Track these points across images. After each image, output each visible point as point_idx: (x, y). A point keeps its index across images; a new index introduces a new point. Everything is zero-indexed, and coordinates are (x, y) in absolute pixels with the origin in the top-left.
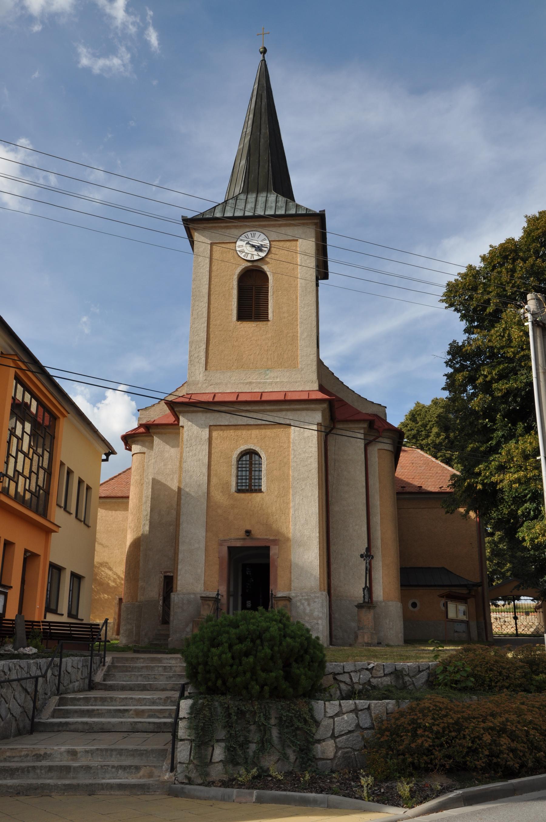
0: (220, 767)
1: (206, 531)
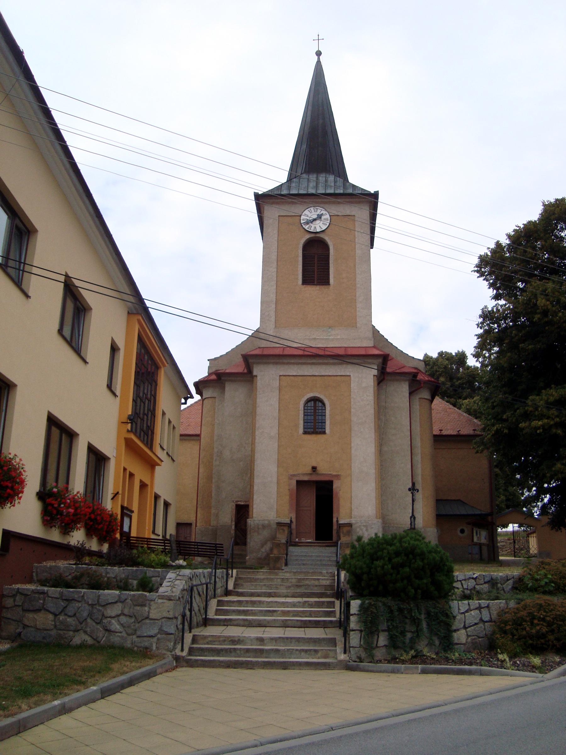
0: (384, 650)
1: (278, 467)
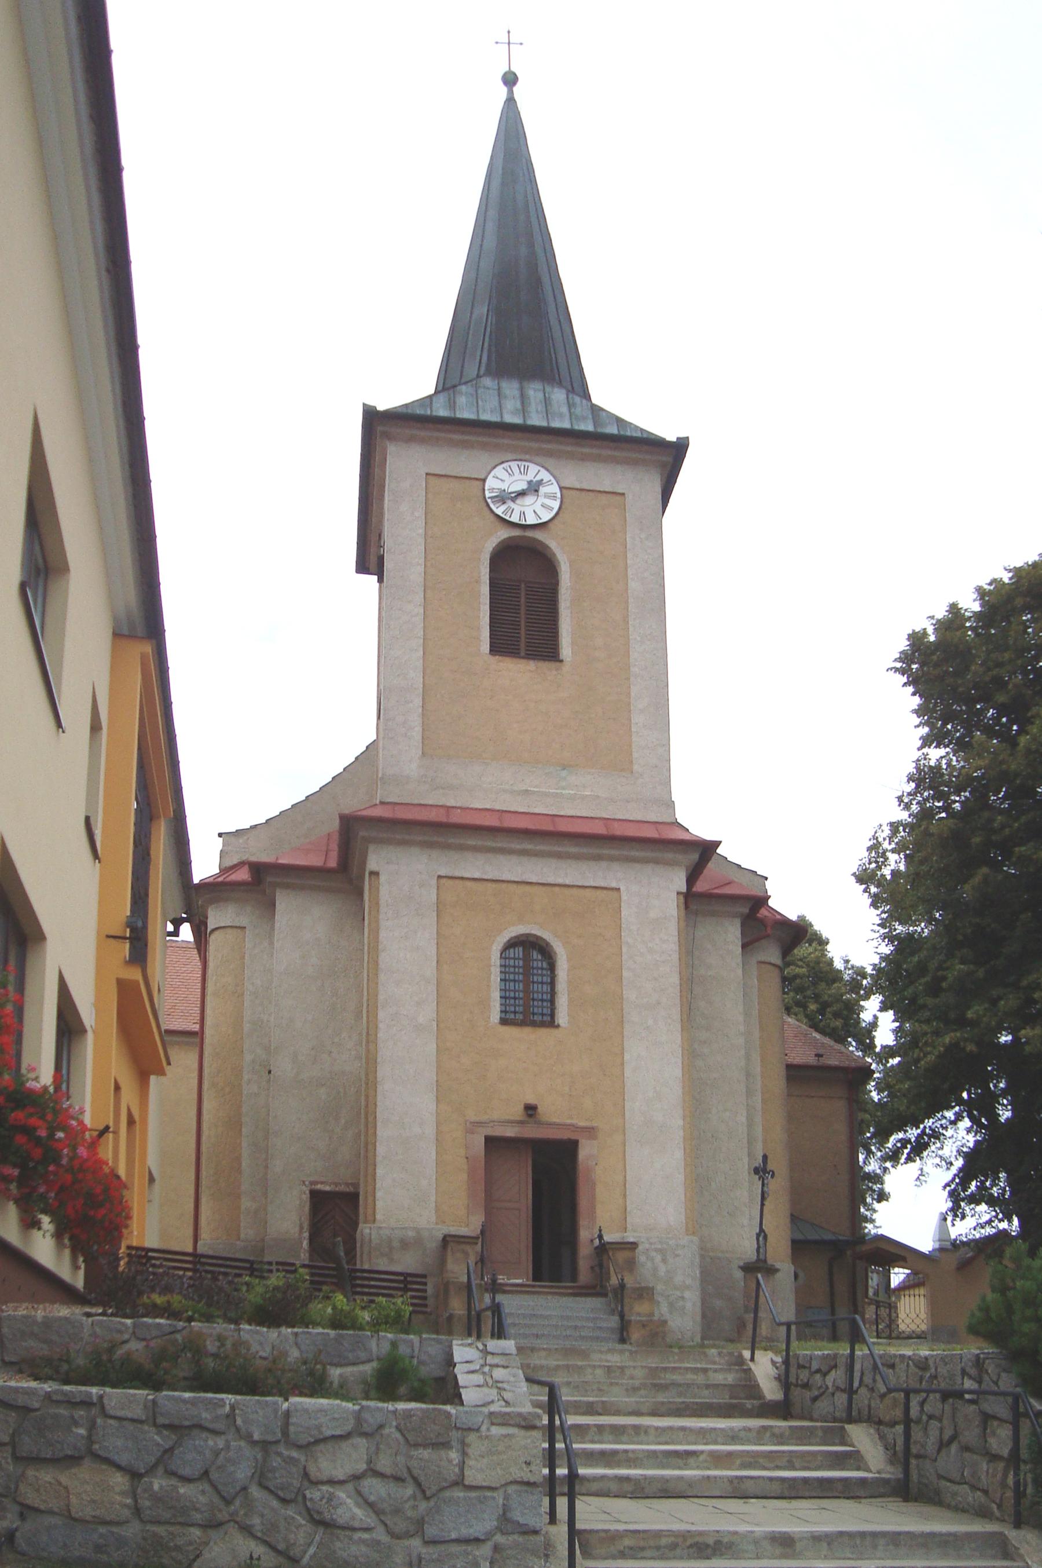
1: (438, 1101)
